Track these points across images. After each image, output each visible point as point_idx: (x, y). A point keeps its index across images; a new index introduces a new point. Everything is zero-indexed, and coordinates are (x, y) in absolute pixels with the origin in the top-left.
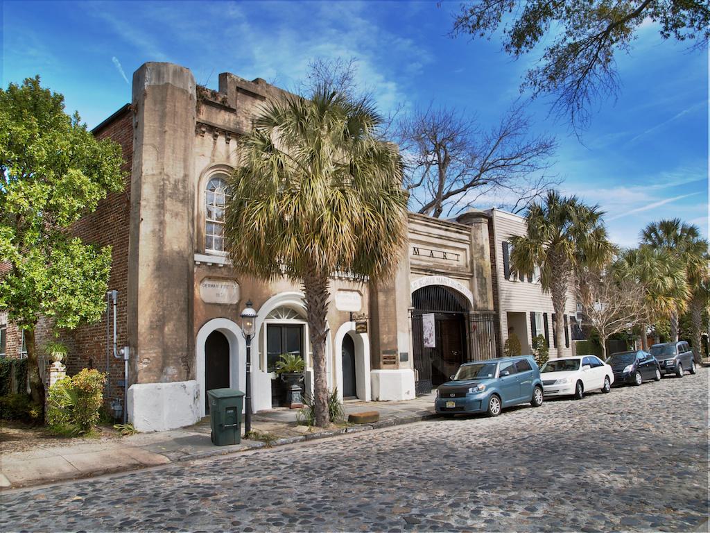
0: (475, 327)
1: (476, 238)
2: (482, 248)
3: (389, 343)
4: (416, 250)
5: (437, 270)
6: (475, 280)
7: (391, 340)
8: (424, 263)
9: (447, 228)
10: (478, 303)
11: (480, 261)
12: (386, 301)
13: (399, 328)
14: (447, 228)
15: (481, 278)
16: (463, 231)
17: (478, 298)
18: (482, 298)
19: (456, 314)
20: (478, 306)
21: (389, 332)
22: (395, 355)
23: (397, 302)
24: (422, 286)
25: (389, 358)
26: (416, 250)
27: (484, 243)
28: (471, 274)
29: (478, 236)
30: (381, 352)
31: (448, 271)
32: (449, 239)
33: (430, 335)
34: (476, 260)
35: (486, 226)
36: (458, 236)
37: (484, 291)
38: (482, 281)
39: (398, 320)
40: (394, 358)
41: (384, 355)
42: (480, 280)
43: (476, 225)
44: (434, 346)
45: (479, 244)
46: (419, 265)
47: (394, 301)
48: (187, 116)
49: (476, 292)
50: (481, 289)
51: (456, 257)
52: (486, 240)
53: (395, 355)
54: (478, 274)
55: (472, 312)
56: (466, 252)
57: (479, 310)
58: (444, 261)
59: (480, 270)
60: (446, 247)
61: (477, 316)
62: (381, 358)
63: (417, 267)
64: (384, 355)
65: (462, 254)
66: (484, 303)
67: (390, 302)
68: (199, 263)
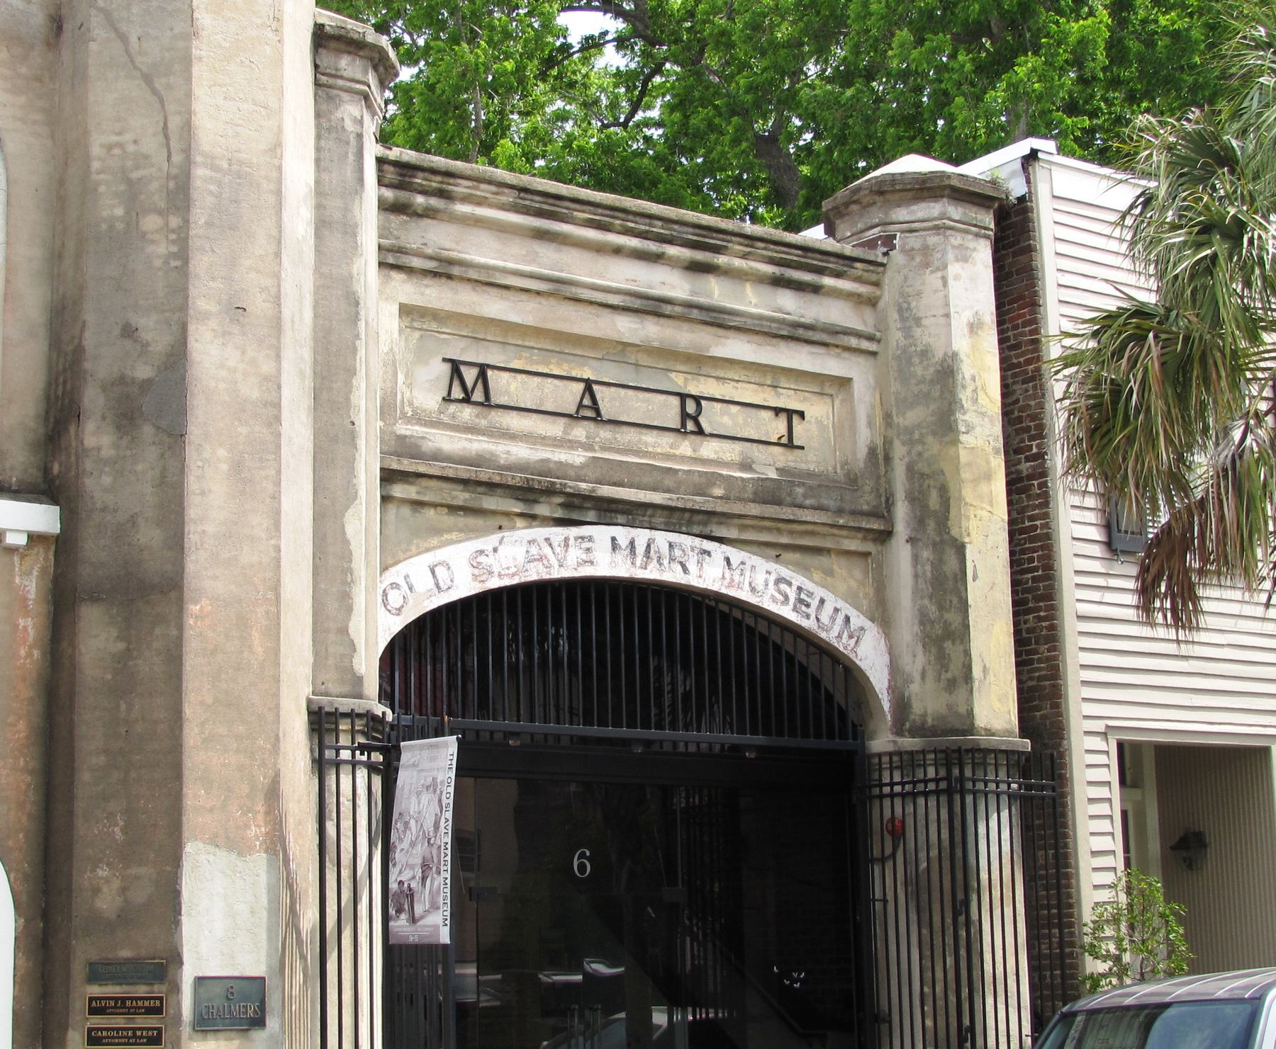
0: (897, 831)
1: (909, 319)
2: (947, 373)
3: (126, 918)
4: (470, 375)
5: (606, 491)
6: (901, 553)
7: (140, 895)
8: (521, 452)
9: (700, 256)
10: (915, 688)
11: (933, 445)
12: (123, 661)
13: (191, 820)
14: (700, 256)
15: (938, 547)
16: (828, 281)
17: (916, 661)
18: (942, 660)
19: (760, 749)
20: (917, 708)
21: (127, 855)
22: (159, 989)
23: (193, 663)
24: (494, 583)
25: (121, 1005)
26: (470, 375)
27: (961, 343)
28: (876, 525)
29: (926, 305)
30: (78, 969)
31: (698, 502)
32: (717, 319)
33: (426, 867)
34: (911, 443)
35: (983, 254)
36: (789, 304)
37: (953, 617)
38: (938, 564)
39: (189, 775)
40: (158, 1011)
41: (96, 990)
42: (926, 554)
43: (914, 241)
44: (445, 937)
45: (925, 353)
46: (477, 461)
47: (174, 658)
48: (155, 92)
49: (907, 628)
50: (932, 609)
51: (777, 428)
52: (974, 327)
53: (159, 989)
54: (919, 521)
55: (882, 741)
56: (849, 400)
57: (914, 732)
58: (685, 447)
59: (934, 501)
60: (699, 362)
61: (907, 760)
62: (79, 1005)
63: (463, 472)
64: (96, 990)
65: (817, 410)
66: (951, 685)
67: (149, 665)
68: (21, 540)
